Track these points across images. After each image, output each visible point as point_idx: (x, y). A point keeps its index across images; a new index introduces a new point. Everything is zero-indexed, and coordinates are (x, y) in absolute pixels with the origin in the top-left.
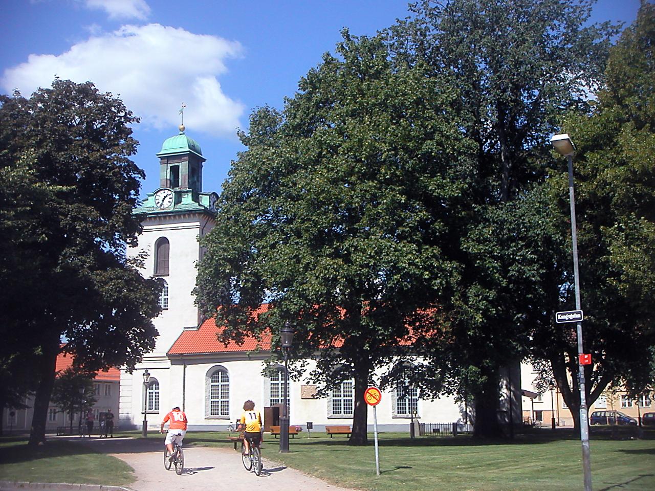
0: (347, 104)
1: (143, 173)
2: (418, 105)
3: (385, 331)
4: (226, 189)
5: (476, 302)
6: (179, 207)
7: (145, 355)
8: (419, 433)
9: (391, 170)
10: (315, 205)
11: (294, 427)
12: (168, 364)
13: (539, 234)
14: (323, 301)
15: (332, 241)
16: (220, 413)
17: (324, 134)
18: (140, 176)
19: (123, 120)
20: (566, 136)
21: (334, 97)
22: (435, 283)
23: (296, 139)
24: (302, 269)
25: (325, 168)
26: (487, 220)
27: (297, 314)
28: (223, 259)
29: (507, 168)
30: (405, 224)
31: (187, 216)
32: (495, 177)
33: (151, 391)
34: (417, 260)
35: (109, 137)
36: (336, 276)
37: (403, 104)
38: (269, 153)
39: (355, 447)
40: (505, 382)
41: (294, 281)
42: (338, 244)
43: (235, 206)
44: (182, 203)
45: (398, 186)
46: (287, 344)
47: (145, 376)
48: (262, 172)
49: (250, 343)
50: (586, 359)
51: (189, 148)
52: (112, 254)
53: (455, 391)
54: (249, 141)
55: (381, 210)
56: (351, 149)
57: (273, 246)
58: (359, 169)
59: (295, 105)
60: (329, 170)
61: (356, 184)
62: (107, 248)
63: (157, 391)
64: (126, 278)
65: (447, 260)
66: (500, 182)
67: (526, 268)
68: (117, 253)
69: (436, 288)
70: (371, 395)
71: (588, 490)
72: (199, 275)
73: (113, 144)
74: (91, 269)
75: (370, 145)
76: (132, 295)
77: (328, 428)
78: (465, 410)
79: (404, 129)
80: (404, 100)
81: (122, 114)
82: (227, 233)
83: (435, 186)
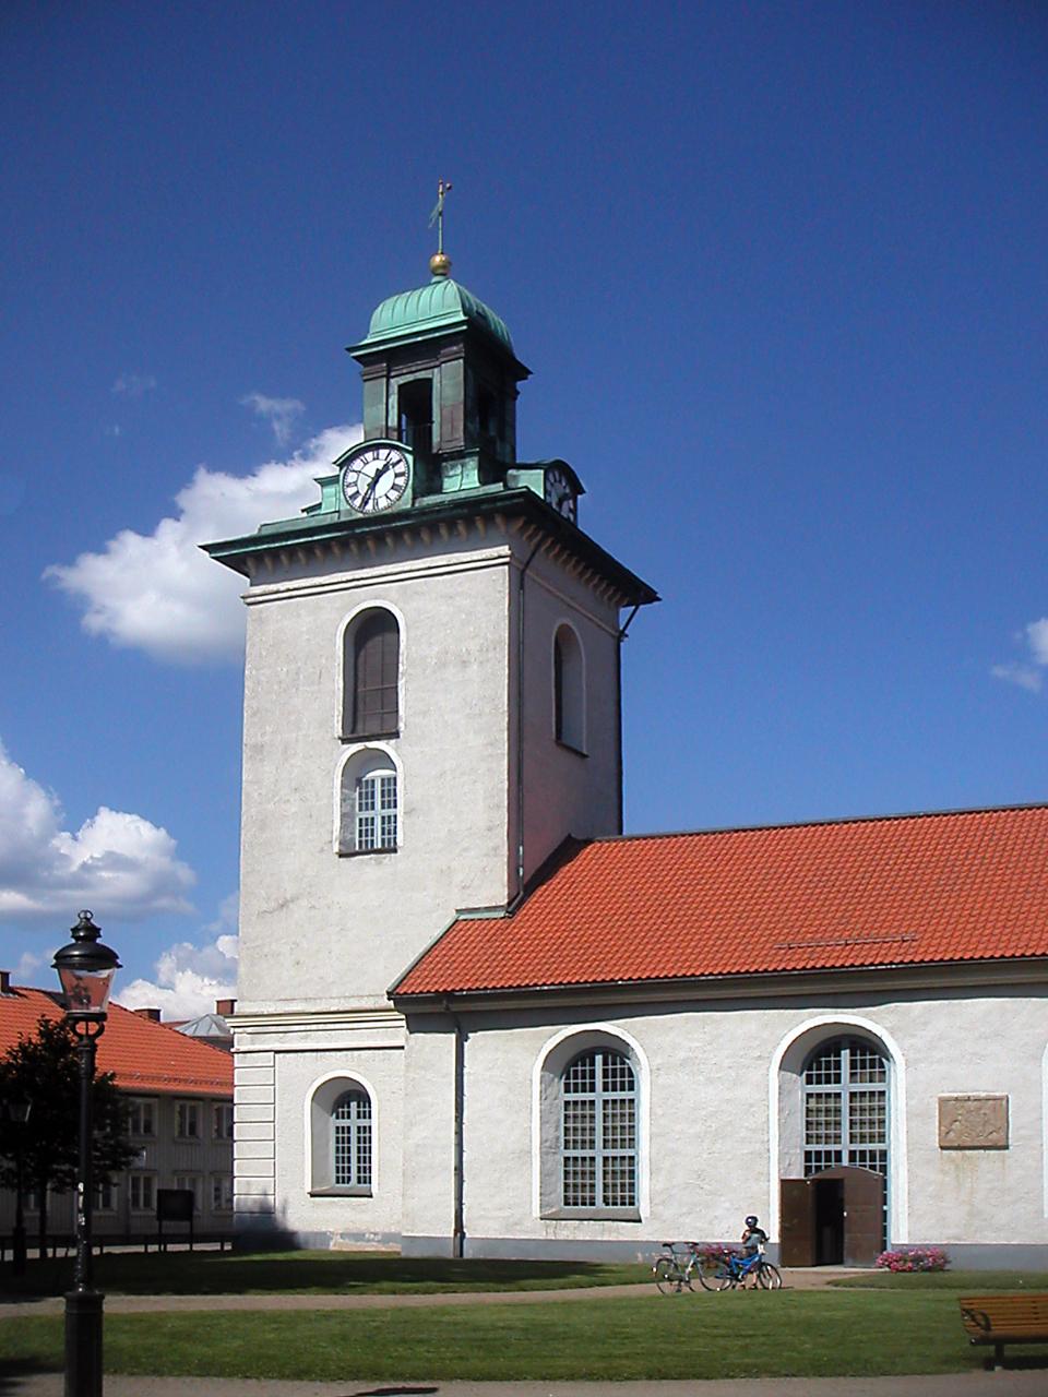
63: (363, 1122)
71: (4, 1054)
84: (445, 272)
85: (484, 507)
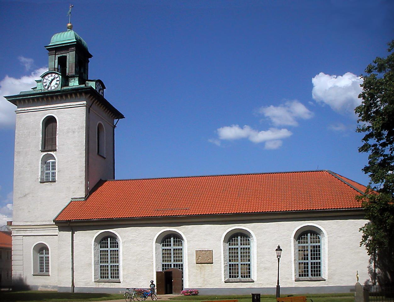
12: (56, 231)
16: (110, 277)
33: (42, 256)
51: (76, 39)
63: (47, 256)
78: (374, 271)
84: (71, 28)
85: (80, 91)
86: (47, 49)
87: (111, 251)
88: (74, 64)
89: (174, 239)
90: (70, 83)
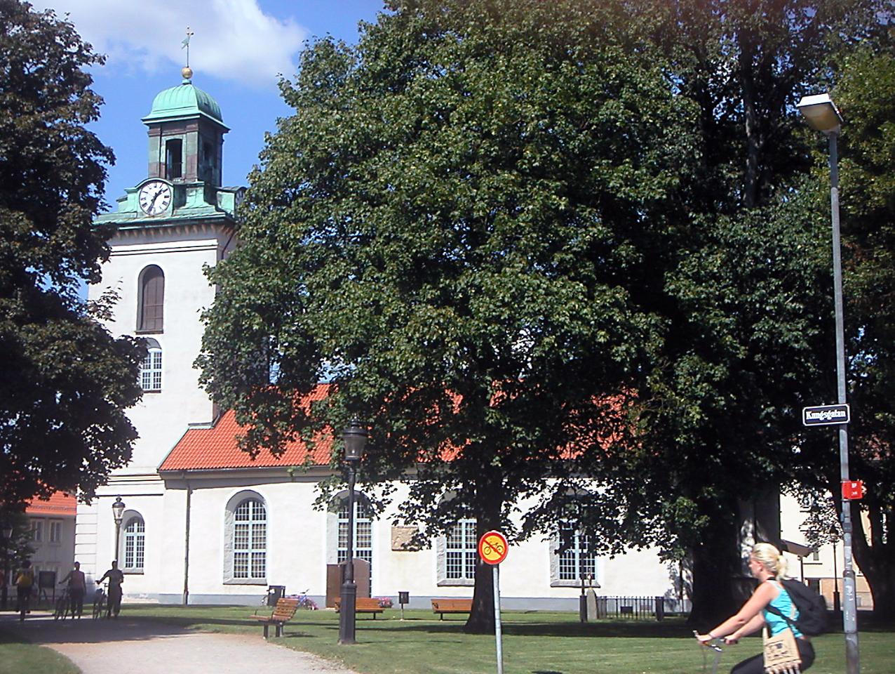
0: (469, 35)
1: (111, 153)
2: (594, 35)
3: (528, 435)
4: (254, 182)
5: (690, 386)
6: (182, 213)
7: (114, 472)
8: (595, 614)
9: (541, 152)
10: (408, 214)
11: (377, 600)
12: (160, 487)
13: (807, 266)
14: (420, 380)
15: (438, 276)
16: (250, 575)
17: (427, 88)
18: (105, 159)
19: (75, 59)
20: (824, 98)
21: (446, 21)
22: (617, 351)
23: (380, 96)
24: (384, 325)
25: (427, 147)
26: (715, 241)
27: (377, 401)
28: (249, 306)
29: (756, 148)
30: (565, 247)
31: (195, 229)
32: (734, 165)
33: (130, 534)
34: (585, 311)
35: (51, 89)
36: (442, 337)
37: (566, 34)
38: (330, 121)
39: (476, 636)
40: (751, 526)
41: (370, 345)
42: (447, 282)
43: (271, 214)
44: (187, 206)
45: (556, 181)
46: (353, 455)
47: (116, 509)
48: (318, 154)
49: (295, 452)
50: (854, 490)
51: (200, 108)
52: (56, 295)
53: (652, 540)
54: (296, 99)
55: (523, 221)
56: (474, 114)
57: (336, 285)
58: (486, 151)
59: (378, 36)
60: (435, 152)
61: (480, 177)
62: (47, 283)
63: (141, 534)
64: (79, 337)
65: (639, 311)
66: (741, 173)
67: (782, 327)
68: (64, 293)
69: (619, 359)
70: (491, 546)
72: (208, 333)
73: (56, 103)
74: (19, 321)
75: (505, 108)
76: (90, 368)
77: (436, 603)
78: (678, 575)
79: (568, 80)
80: (569, 27)
81: (74, 49)
82: (255, 261)
83: (621, 181)
85: (206, 221)
86: (147, 124)
87: (253, 525)
88: (196, 157)
89: (358, 504)
90: (188, 198)
